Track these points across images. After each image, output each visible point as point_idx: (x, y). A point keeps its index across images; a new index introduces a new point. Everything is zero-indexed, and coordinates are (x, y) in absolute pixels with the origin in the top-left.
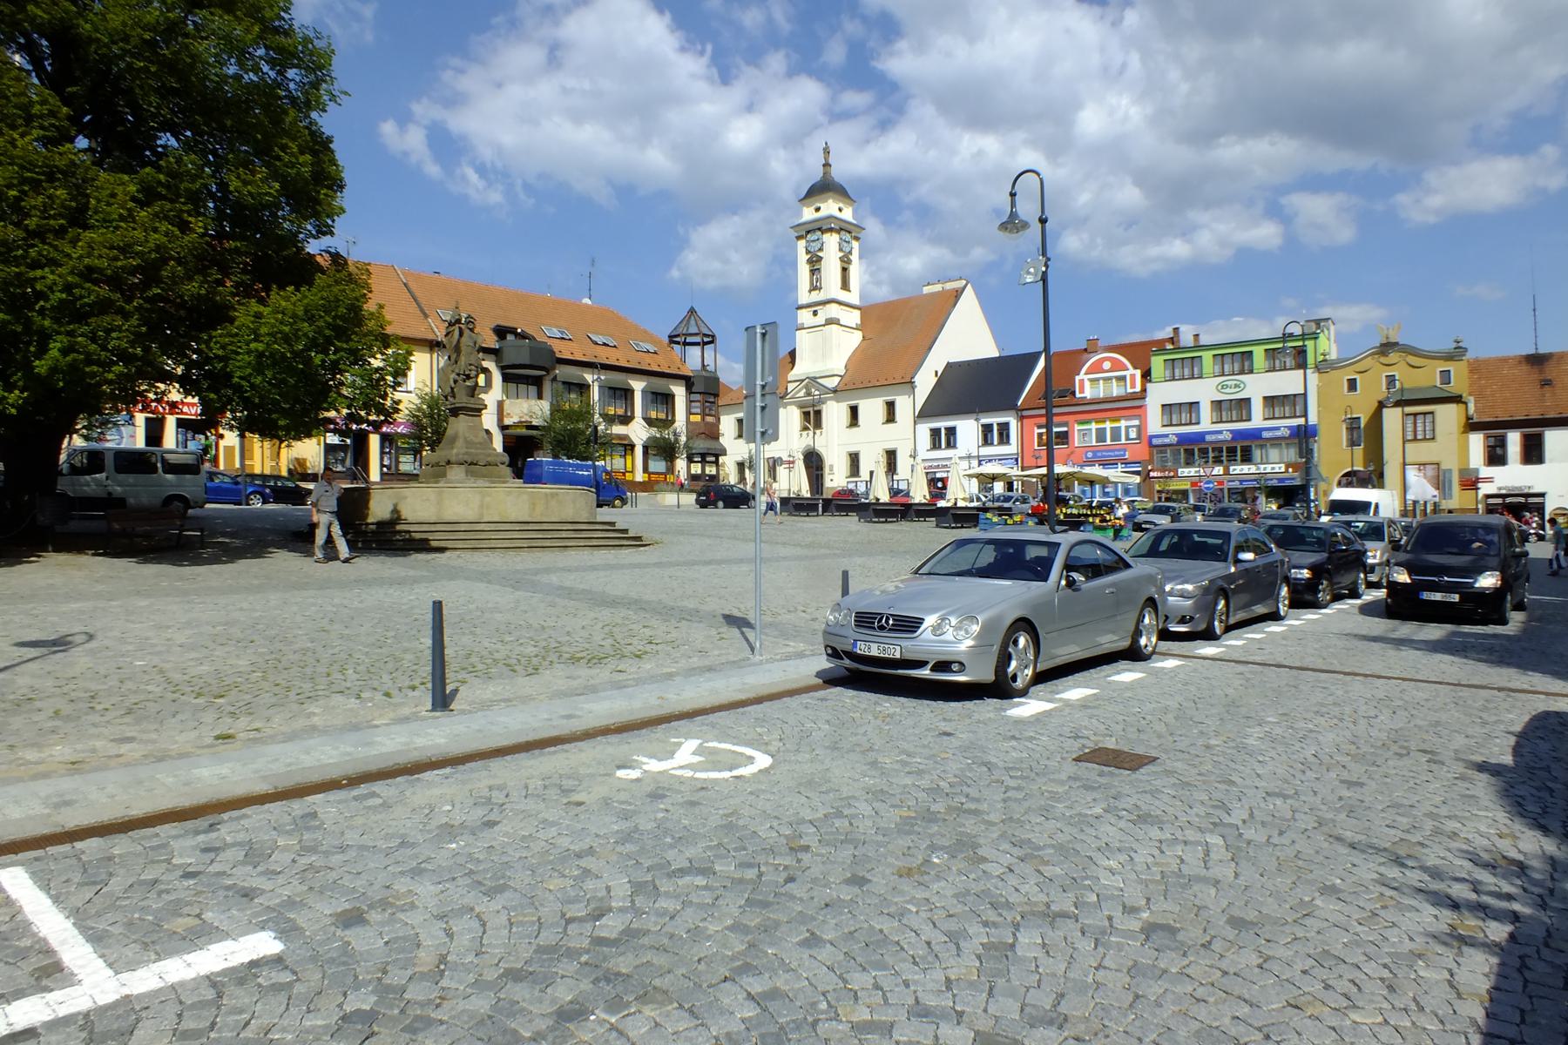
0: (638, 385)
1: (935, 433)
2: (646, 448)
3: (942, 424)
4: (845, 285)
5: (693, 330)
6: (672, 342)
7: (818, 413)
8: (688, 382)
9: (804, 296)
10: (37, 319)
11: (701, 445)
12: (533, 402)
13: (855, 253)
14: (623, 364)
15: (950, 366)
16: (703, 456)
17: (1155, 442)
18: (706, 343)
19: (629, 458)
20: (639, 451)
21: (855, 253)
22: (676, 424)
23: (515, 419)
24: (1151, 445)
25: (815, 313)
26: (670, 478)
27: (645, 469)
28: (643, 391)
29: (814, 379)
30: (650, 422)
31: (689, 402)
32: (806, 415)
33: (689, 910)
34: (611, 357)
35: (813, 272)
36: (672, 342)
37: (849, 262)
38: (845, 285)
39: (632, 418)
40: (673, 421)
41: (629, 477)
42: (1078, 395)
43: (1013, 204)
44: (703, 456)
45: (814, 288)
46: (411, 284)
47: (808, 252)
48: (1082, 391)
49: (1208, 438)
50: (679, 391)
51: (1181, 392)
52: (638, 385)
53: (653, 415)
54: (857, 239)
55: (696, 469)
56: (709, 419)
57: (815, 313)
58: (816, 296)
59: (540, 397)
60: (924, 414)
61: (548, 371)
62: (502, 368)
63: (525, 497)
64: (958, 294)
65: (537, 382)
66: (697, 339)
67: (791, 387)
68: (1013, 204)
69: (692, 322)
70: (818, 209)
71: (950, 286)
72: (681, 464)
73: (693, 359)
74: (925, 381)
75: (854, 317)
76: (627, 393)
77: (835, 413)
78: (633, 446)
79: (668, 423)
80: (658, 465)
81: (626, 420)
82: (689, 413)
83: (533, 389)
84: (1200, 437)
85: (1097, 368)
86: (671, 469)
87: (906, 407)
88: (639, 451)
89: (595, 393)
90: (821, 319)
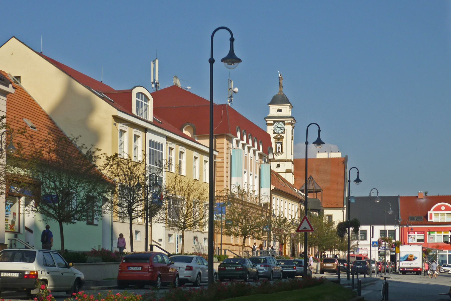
25: (278, 166)
42: (429, 220)
48: (431, 218)
85: (438, 209)
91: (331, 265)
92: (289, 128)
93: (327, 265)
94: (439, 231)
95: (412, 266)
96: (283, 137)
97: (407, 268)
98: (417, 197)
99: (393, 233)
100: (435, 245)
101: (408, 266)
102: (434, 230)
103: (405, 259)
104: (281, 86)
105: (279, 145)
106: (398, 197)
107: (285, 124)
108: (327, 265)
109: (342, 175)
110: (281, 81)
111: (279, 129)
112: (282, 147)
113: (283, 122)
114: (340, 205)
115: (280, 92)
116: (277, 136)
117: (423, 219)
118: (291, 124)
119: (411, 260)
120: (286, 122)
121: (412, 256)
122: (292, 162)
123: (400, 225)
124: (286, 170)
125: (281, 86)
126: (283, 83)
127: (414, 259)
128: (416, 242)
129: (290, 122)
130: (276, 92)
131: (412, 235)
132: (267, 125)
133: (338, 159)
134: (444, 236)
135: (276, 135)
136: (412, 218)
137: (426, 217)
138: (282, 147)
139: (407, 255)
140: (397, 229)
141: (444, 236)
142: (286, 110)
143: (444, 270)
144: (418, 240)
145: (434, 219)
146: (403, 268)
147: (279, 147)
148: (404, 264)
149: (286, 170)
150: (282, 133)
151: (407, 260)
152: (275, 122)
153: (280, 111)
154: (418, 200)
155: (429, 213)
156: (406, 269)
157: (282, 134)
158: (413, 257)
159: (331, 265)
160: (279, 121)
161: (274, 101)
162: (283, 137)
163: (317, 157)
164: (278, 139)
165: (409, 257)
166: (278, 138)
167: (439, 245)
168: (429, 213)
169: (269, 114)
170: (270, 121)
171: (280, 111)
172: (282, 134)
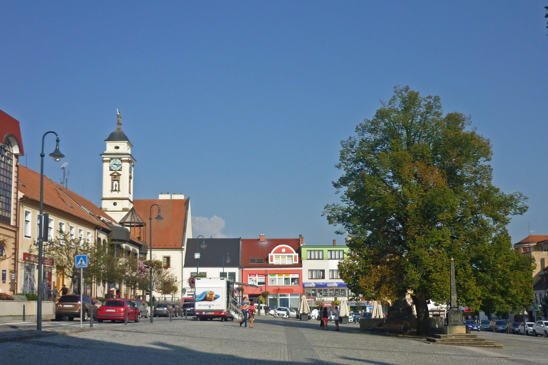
9: (107, 192)
10: (178, 270)
17: (306, 286)
24: (303, 286)
25: (115, 204)
42: (270, 262)
43: (57, 145)
47: (111, 170)
48: (272, 261)
49: (328, 285)
51: (317, 265)
57: (115, 204)
58: (115, 195)
68: (57, 145)
84: (325, 285)
85: (279, 251)
91: (71, 306)
92: (126, 166)
93: (65, 306)
94: (280, 273)
95: (212, 308)
96: (119, 175)
97: (206, 311)
98: (259, 239)
99: (233, 275)
100: (276, 288)
101: (207, 308)
102: (273, 273)
103: (202, 298)
104: (119, 124)
105: (116, 182)
106: (239, 239)
107: (122, 161)
108: (65, 306)
109: (183, 216)
110: (120, 119)
111: (116, 166)
112: (119, 185)
113: (120, 159)
114: (179, 246)
115: (119, 129)
116: (114, 173)
117: (264, 262)
118: (129, 161)
119: (210, 300)
120: (123, 159)
121: (211, 294)
122: (130, 200)
123: (240, 267)
124: (123, 209)
125: (119, 124)
126: (121, 121)
127: (215, 299)
128: (257, 285)
129: (127, 159)
130: (114, 129)
131: (253, 278)
132: (104, 161)
133: (181, 200)
134: (285, 279)
136: (253, 261)
137: (267, 259)
138: (119, 185)
139: (205, 293)
140: (236, 270)
141: (285, 279)
142: (124, 147)
143: (278, 314)
144: (259, 283)
145: (275, 262)
146: (201, 311)
147: (116, 185)
148: (200, 306)
149: (123, 209)
150: (119, 170)
151: (205, 299)
152: (112, 159)
153: (117, 148)
154: (260, 243)
155: (270, 255)
156: (204, 313)
157: (118, 172)
158: (214, 296)
159: (71, 306)
160: (116, 158)
161: (112, 138)
162: (119, 175)
163: (160, 198)
164: (115, 177)
165: (208, 296)
166: (115, 176)
167: (280, 288)
168: (270, 255)
169: (105, 150)
170: (106, 158)
171: (117, 148)
172: (118, 172)
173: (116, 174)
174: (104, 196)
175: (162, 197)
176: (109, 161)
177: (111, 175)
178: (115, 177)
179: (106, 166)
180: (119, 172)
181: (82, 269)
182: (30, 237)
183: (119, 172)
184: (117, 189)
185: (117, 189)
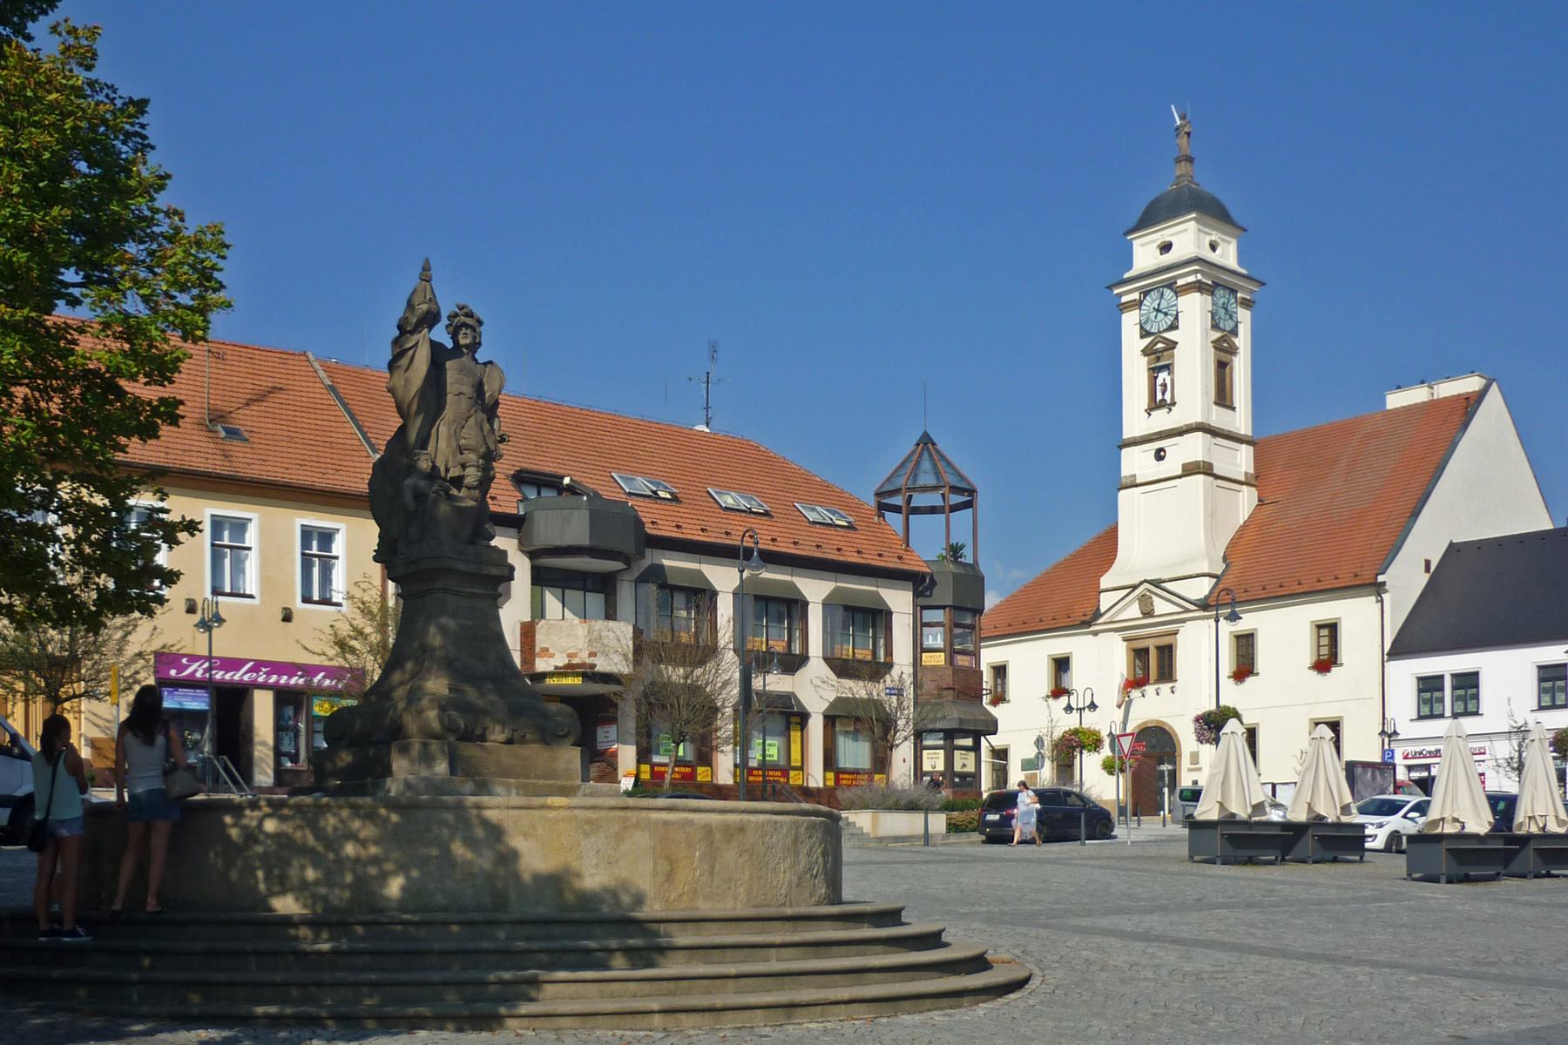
0: (815, 590)
1: (1429, 686)
2: (830, 720)
3: (1447, 665)
4: (1223, 397)
5: (927, 479)
6: (882, 508)
7: (1167, 653)
8: (919, 583)
9: (1135, 420)
11: (953, 715)
12: (600, 624)
13: (1244, 331)
14: (784, 547)
15: (1454, 550)
16: (950, 734)
18: (954, 508)
19: (795, 735)
20: (816, 726)
21: (1244, 331)
22: (895, 672)
23: (561, 661)
25: (1160, 455)
26: (702, 774)
27: (830, 761)
28: (827, 605)
29: (1157, 583)
30: (842, 668)
31: (919, 626)
32: (1140, 654)
33: (157, 205)
34: (767, 537)
35: (1154, 371)
36: (882, 508)
37: (1233, 351)
38: (1223, 397)
39: (803, 659)
40: (889, 666)
41: (795, 779)
44: (950, 734)
45: (1155, 405)
46: (341, 388)
47: (1145, 333)
50: (899, 601)
52: (815, 590)
53: (847, 651)
54: (1246, 304)
55: (934, 761)
56: (962, 661)
57: (1160, 455)
58: (1163, 420)
59: (610, 614)
60: (1402, 647)
61: (627, 560)
62: (532, 555)
63: (641, 839)
64: (1471, 403)
65: (605, 585)
66: (934, 499)
67: (1106, 601)
69: (926, 464)
70: (1166, 248)
71: (1448, 389)
72: (902, 754)
73: (927, 543)
74: (1407, 579)
75: (1241, 461)
76: (794, 607)
77: (1200, 648)
78: (803, 717)
79: (877, 669)
80: (855, 753)
81: (793, 663)
82: (919, 649)
83: (596, 601)
86: (881, 763)
87: (1363, 623)
88: (816, 726)
89: (725, 609)
90: (1172, 465)
96: (1172, 345)
112: (1172, 381)
116: (1153, 344)
124: (1184, 466)
129: (1191, 279)
130: (1163, 184)
135: (1149, 340)
138: (1172, 381)
149: (1184, 466)
152: (1146, 294)
157: (1166, 335)
161: (1152, 217)
162: (1172, 345)
163: (1389, 407)
169: (1130, 267)
173: (1160, 345)
174: (1127, 434)
175: (1395, 400)
176: (1138, 304)
177: (1146, 352)
178: (1160, 357)
179: (1130, 321)
180: (1170, 335)
181: (1448, 713)
182: (251, 597)
183: (1170, 335)
184: (1168, 397)
185: (1168, 397)
